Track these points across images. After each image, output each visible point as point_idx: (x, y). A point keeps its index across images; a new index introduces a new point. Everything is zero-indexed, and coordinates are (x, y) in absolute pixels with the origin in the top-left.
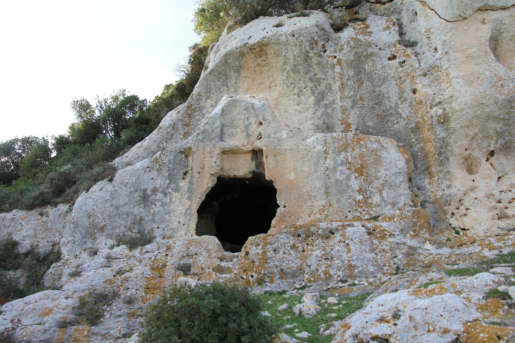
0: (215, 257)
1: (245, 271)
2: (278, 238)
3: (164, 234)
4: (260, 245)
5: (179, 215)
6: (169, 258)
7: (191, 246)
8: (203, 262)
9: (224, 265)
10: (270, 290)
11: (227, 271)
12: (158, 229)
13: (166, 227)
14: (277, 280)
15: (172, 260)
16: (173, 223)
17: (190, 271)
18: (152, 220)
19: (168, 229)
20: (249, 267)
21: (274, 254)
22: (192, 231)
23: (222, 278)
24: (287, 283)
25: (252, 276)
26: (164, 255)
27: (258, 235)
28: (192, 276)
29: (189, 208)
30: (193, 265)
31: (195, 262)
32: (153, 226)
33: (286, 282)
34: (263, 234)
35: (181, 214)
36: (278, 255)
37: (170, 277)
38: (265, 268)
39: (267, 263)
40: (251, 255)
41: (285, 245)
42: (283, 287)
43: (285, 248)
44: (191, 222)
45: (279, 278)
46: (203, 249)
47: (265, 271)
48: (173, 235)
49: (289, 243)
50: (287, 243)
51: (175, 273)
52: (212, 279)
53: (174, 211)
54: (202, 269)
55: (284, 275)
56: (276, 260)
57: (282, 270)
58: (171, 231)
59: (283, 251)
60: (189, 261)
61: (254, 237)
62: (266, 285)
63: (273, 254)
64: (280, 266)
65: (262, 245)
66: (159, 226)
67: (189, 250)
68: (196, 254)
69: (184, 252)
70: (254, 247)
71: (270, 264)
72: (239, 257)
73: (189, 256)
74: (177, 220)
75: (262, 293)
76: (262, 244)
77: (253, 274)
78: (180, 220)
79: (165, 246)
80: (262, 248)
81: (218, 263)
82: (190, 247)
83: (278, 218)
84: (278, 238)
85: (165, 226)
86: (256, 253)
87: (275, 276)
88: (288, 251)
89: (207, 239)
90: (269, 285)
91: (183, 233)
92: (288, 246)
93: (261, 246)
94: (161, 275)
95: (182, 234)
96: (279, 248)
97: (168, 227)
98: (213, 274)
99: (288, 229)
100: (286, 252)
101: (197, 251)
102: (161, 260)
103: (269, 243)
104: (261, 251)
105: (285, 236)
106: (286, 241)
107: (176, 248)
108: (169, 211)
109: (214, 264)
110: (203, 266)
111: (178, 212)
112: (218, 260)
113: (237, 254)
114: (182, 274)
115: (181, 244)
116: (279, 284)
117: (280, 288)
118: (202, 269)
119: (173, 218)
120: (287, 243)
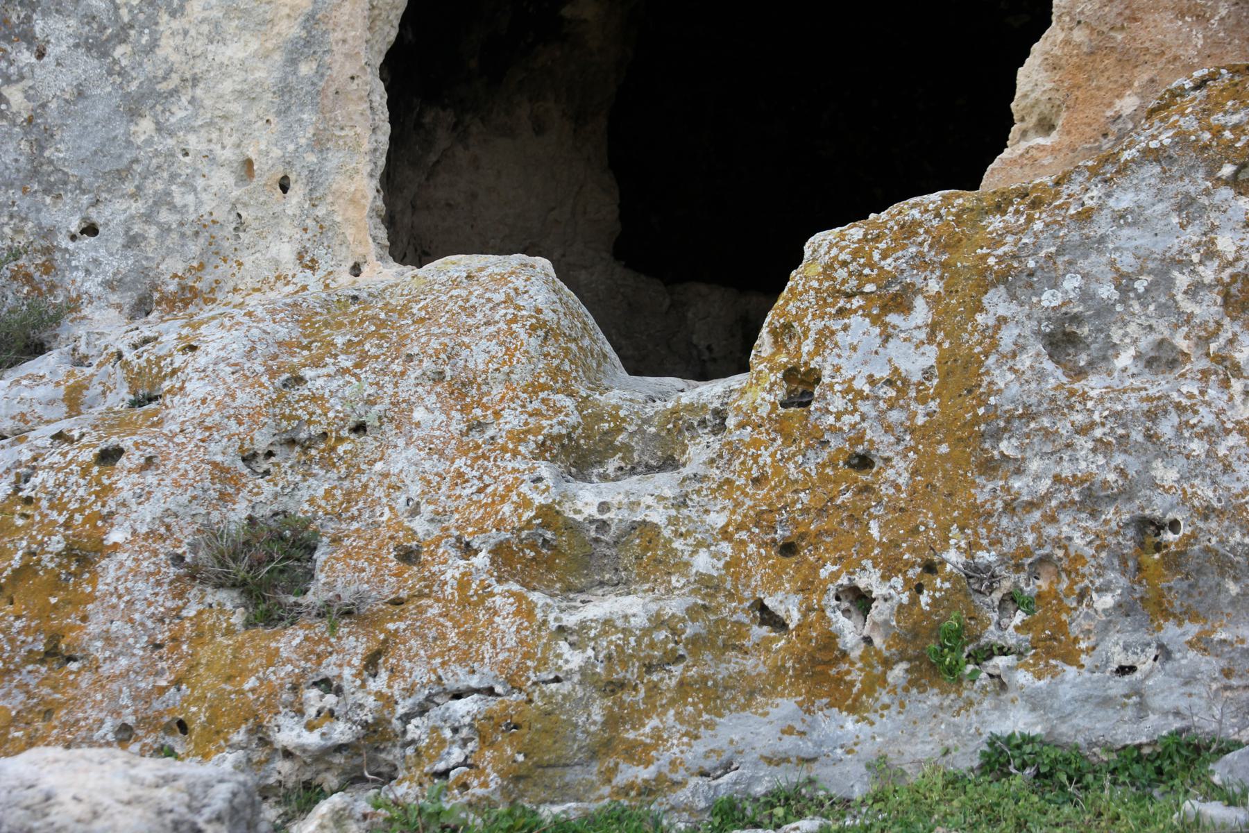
0: (518, 437)
1: (788, 549)
2: (1086, 216)
3: (145, 272)
4: (919, 302)
5: (237, 108)
6: (124, 480)
7: (316, 363)
8: (415, 489)
9: (592, 511)
10: (1037, 730)
11: (627, 559)
12: (88, 240)
13: (148, 218)
14: (1106, 628)
15: (144, 496)
16: (200, 183)
17: (301, 582)
18: (35, 173)
19: (165, 230)
20: (821, 512)
21: (1055, 375)
22: (350, 232)
23: (577, 636)
24: (1209, 665)
25: (861, 600)
26: (88, 455)
27: (894, 209)
28: (321, 627)
29: (307, 43)
30: (331, 528)
31: (349, 497)
32: (47, 219)
33: (1202, 644)
34: (936, 196)
35: (247, 95)
36: (1094, 384)
37: (128, 651)
38: (978, 514)
39: (989, 467)
40: (838, 403)
41: (1162, 280)
42: (1175, 699)
43: (1169, 308)
44: (334, 159)
45: (1124, 609)
46: (413, 375)
47: (973, 546)
48: (208, 277)
49: (1210, 254)
50: (1181, 263)
51: (177, 614)
52: (487, 649)
53: (195, 81)
54: (408, 556)
55: (1175, 581)
56: (1083, 430)
57: (1148, 527)
58: (194, 248)
59: (1146, 342)
60: (304, 494)
61: (855, 232)
62: (1000, 684)
63: (1042, 376)
64: (1126, 493)
65: (934, 301)
66: (93, 214)
67: (294, 394)
68: (360, 428)
69: (255, 414)
70: (856, 321)
71: (1019, 472)
72: (731, 422)
73: (306, 447)
74: (228, 154)
75: (966, 760)
76: (934, 286)
77: (862, 582)
78: (252, 153)
79: (120, 373)
80: (933, 328)
81: (539, 500)
82: (308, 373)
83: (1079, 35)
84: (1086, 216)
85: (138, 207)
86: (883, 373)
87: (1083, 595)
88: (1204, 341)
89: (456, 283)
90: (1023, 678)
91: (285, 252)
92: (1193, 291)
93: (921, 312)
94: (54, 638)
95: (276, 263)
96: (1104, 310)
97: (164, 216)
98: (503, 596)
99: (1189, 123)
100: (1182, 344)
101: (370, 402)
102: (59, 506)
103: (1002, 278)
104: (930, 356)
105: (1159, 195)
106: (1176, 244)
107: (196, 388)
108: (153, 80)
109: (507, 509)
110: (420, 525)
111: (227, 86)
112: (544, 469)
113: (710, 392)
114: (238, 619)
115: (237, 351)
116: (1123, 670)
117: (1143, 709)
118: (408, 556)
119: (194, 142)
120: (1181, 263)
